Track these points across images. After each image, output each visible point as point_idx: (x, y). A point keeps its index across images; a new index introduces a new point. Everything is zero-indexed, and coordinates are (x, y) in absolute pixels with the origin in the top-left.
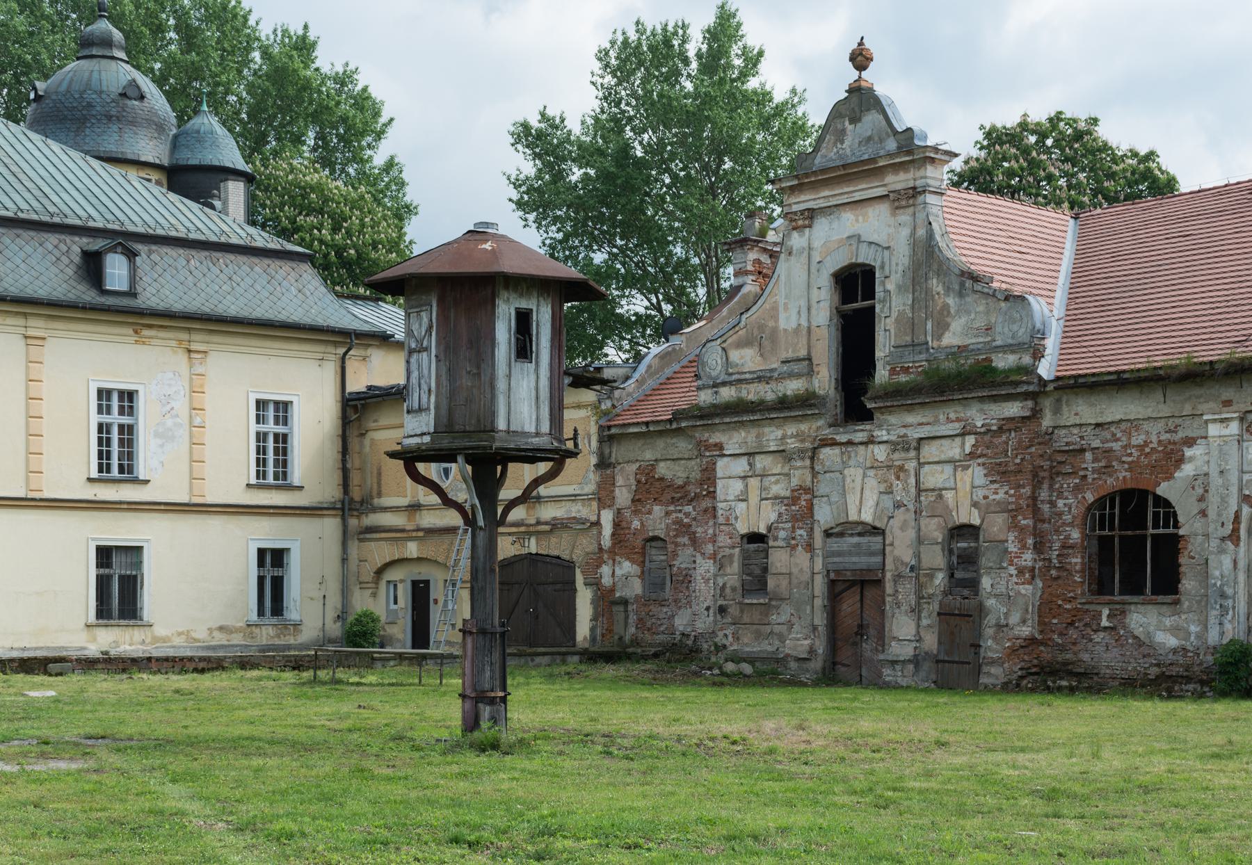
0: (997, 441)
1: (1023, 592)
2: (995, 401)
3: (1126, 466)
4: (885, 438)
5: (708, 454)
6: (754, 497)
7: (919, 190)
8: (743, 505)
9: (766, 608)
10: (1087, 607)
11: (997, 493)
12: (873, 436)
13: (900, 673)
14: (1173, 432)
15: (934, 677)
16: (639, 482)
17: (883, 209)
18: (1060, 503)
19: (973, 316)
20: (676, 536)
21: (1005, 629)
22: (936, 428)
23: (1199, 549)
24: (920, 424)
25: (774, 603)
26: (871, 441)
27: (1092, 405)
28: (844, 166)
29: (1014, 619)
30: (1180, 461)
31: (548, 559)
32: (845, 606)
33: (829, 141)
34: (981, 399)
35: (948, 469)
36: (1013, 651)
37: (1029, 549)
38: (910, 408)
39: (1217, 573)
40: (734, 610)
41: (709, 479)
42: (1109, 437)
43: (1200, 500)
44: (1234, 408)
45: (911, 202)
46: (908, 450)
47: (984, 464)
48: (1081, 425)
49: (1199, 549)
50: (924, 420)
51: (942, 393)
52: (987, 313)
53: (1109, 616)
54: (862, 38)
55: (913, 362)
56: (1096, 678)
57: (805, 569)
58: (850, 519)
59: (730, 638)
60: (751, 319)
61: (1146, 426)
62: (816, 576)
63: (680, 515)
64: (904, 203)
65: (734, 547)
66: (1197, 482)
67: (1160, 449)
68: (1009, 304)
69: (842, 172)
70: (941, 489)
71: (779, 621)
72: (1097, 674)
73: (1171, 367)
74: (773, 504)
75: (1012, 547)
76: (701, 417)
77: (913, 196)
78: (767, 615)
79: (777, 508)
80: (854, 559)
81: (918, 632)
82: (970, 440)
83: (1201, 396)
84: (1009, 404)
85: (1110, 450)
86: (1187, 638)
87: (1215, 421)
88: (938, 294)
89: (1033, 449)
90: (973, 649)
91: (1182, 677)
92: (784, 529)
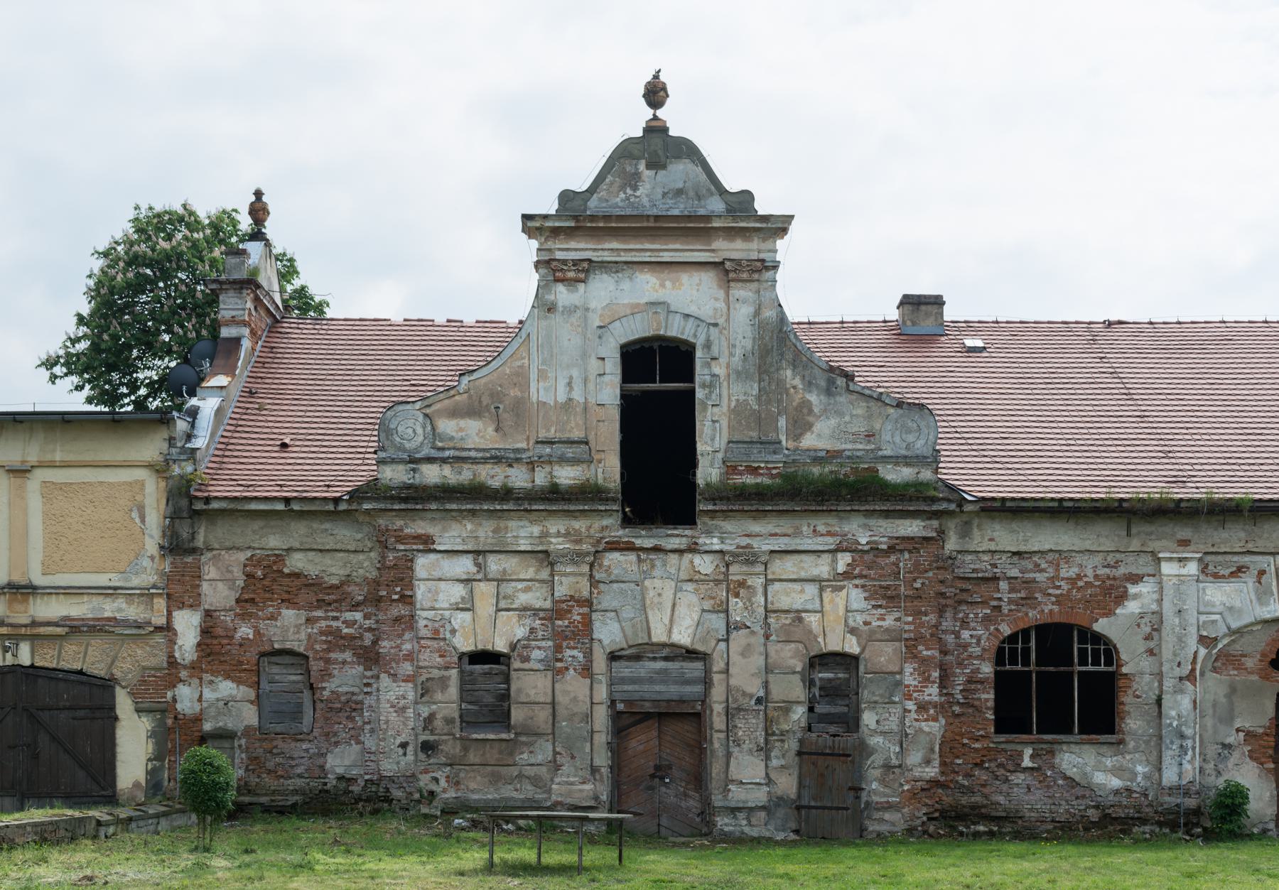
0: (882, 561)
1: (927, 729)
2: (887, 517)
3: (1053, 599)
4: (717, 548)
5: (402, 547)
6: (485, 605)
7: (767, 264)
8: (467, 616)
10: (1003, 746)
11: (884, 620)
12: (696, 544)
13: (744, 822)
14: (1113, 567)
15: (794, 826)
16: (249, 576)
17: (707, 279)
18: (966, 634)
19: (847, 418)
20: (329, 650)
22: (798, 541)
23: (1146, 688)
24: (772, 535)
25: (523, 739)
26: (693, 549)
29: (914, 758)
30: (1122, 597)
31: (53, 674)
32: (633, 744)
33: (612, 183)
34: (870, 514)
35: (811, 590)
36: (913, 795)
37: (934, 682)
38: (759, 515)
39: (1173, 713)
40: (450, 748)
41: (402, 580)
42: (1031, 566)
43: (1146, 639)
44: (1192, 548)
45: (756, 276)
49: (1146, 688)
50: (777, 530)
51: (822, 503)
53: (1032, 757)
55: (767, 462)
57: (581, 698)
58: (655, 640)
59: (443, 783)
60: (477, 383)
61: (1078, 559)
62: (595, 707)
63: (334, 624)
64: (745, 276)
65: (447, 668)
66: (1143, 621)
67: (1097, 583)
70: (798, 611)
71: (532, 761)
72: (1020, 818)
73: (1140, 500)
74: (520, 617)
75: (910, 679)
76: (405, 500)
78: (511, 754)
79: (528, 621)
80: (657, 688)
81: (767, 774)
82: (844, 560)
83: (1151, 534)
84: (907, 522)
85: (1034, 581)
86: (1133, 779)
87: (1171, 559)
88: (794, 387)
89: (930, 574)
90: (852, 793)
91: (1132, 818)
92: (539, 648)
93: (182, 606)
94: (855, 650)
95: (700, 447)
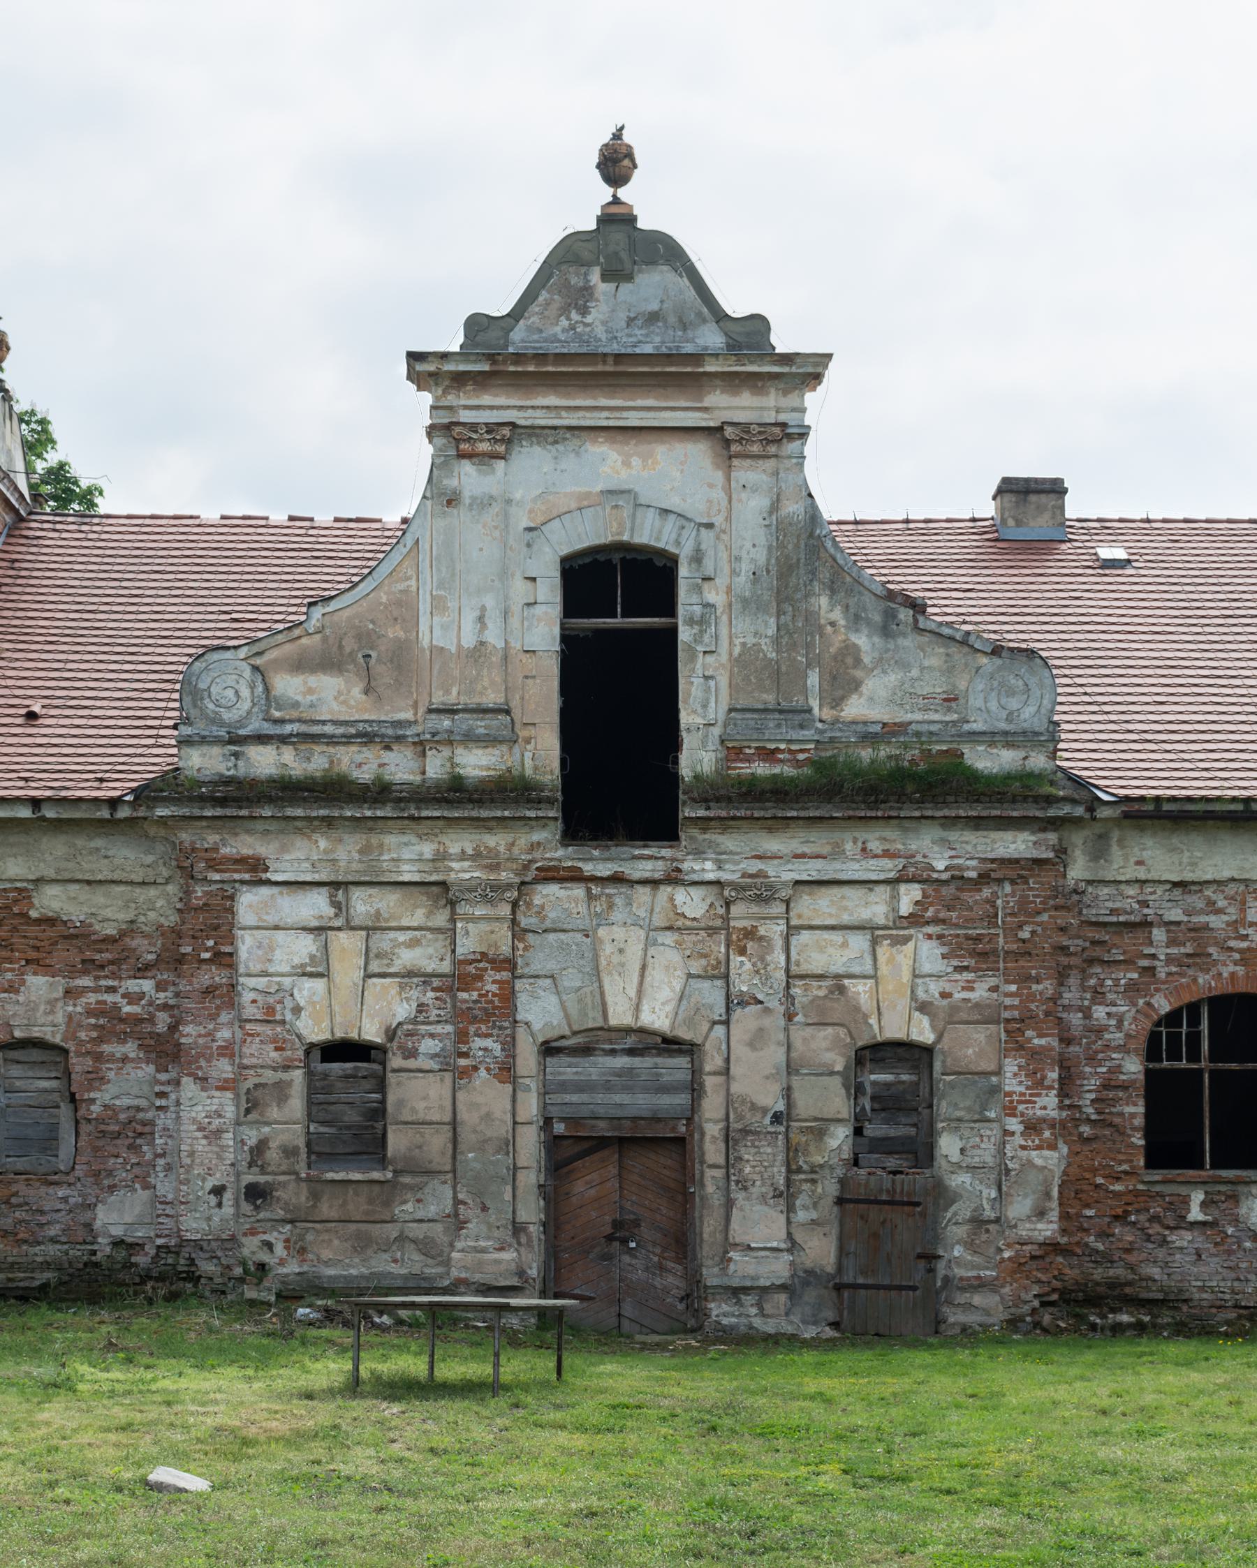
0: (969, 897)
1: (1039, 1162)
2: (977, 828)
3: (1237, 956)
4: (711, 876)
5: (217, 877)
6: (347, 969)
7: (790, 431)
8: (319, 985)
9: (389, 1191)
10: (1158, 1188)
11: (972, 989)
12: (679, 870)
13: (754, 1311)
15: (831, 1315)
17: (698, 453)
18: (1100, 1012)
19: (915, 673)
20: (100, 1040)
21: (991, 1227)
22: (837, 865)
24: (797, 856)
25: (406, 1179)
26: (674, 878)
27: (1173, 850)
28: (619, 358)
29: (1019, 1207)
32: (579, 1187)
33: (547, 304)
34: (950, 822)
35: (859, 942)
36: (1018, 1266)
37: (1051, 1088)
40: (292, 1194)
41: (216, 928)
42: (1201, 904)
45: (772, 449)
46: (767, 901)
47: (940, 937)
48: (1143, 882)
50: (806, 849)
51: (874, 805)
52: (950, 671)
54: (622, 128)
55: (790, 741)
56: (1185, 1308)
58: (613, 1022)
59: (280, 1250)
60: (336, 617)
62: (520, 1129)
64: (755, 449)
65: (286, 1068)
68: (998, 661)
69: (609, 368)
70: (838, 977)
72: (1185, 1301)
74: (402, 987)
75: (1013, 1083)
76: (223, 802)
77: (778, 441)
78: (387, 1204)
79: (414, 994)
80: (617, 1098)
81: (789, 1234)
82: (909, 896)
84: (1008, 835)
85: (1206, 927)
88: (833, 624)
89: (1045, 917)
90: (922, 1264)
92: (432, 1036)
95: (685, 718)
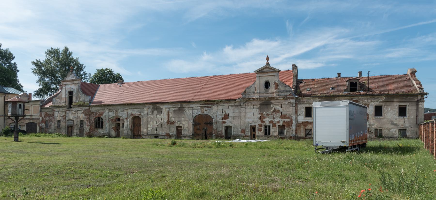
9: (60, 129)
17: (74, 85)
18: (92, 118)
26: (72, 110)
30: (103, 114)
61: (100, 110)
75: (87, 123)
82: (83, 111)
93: (41, 117)
94: (83, 120)
95: (73, 101)
